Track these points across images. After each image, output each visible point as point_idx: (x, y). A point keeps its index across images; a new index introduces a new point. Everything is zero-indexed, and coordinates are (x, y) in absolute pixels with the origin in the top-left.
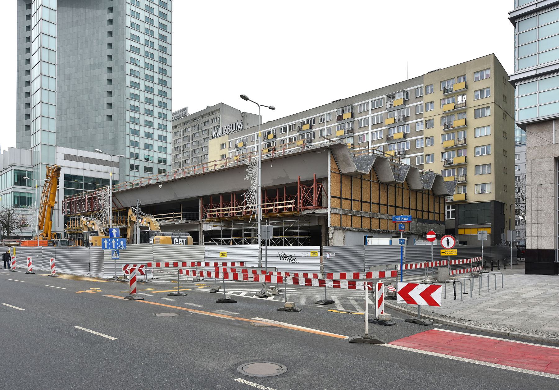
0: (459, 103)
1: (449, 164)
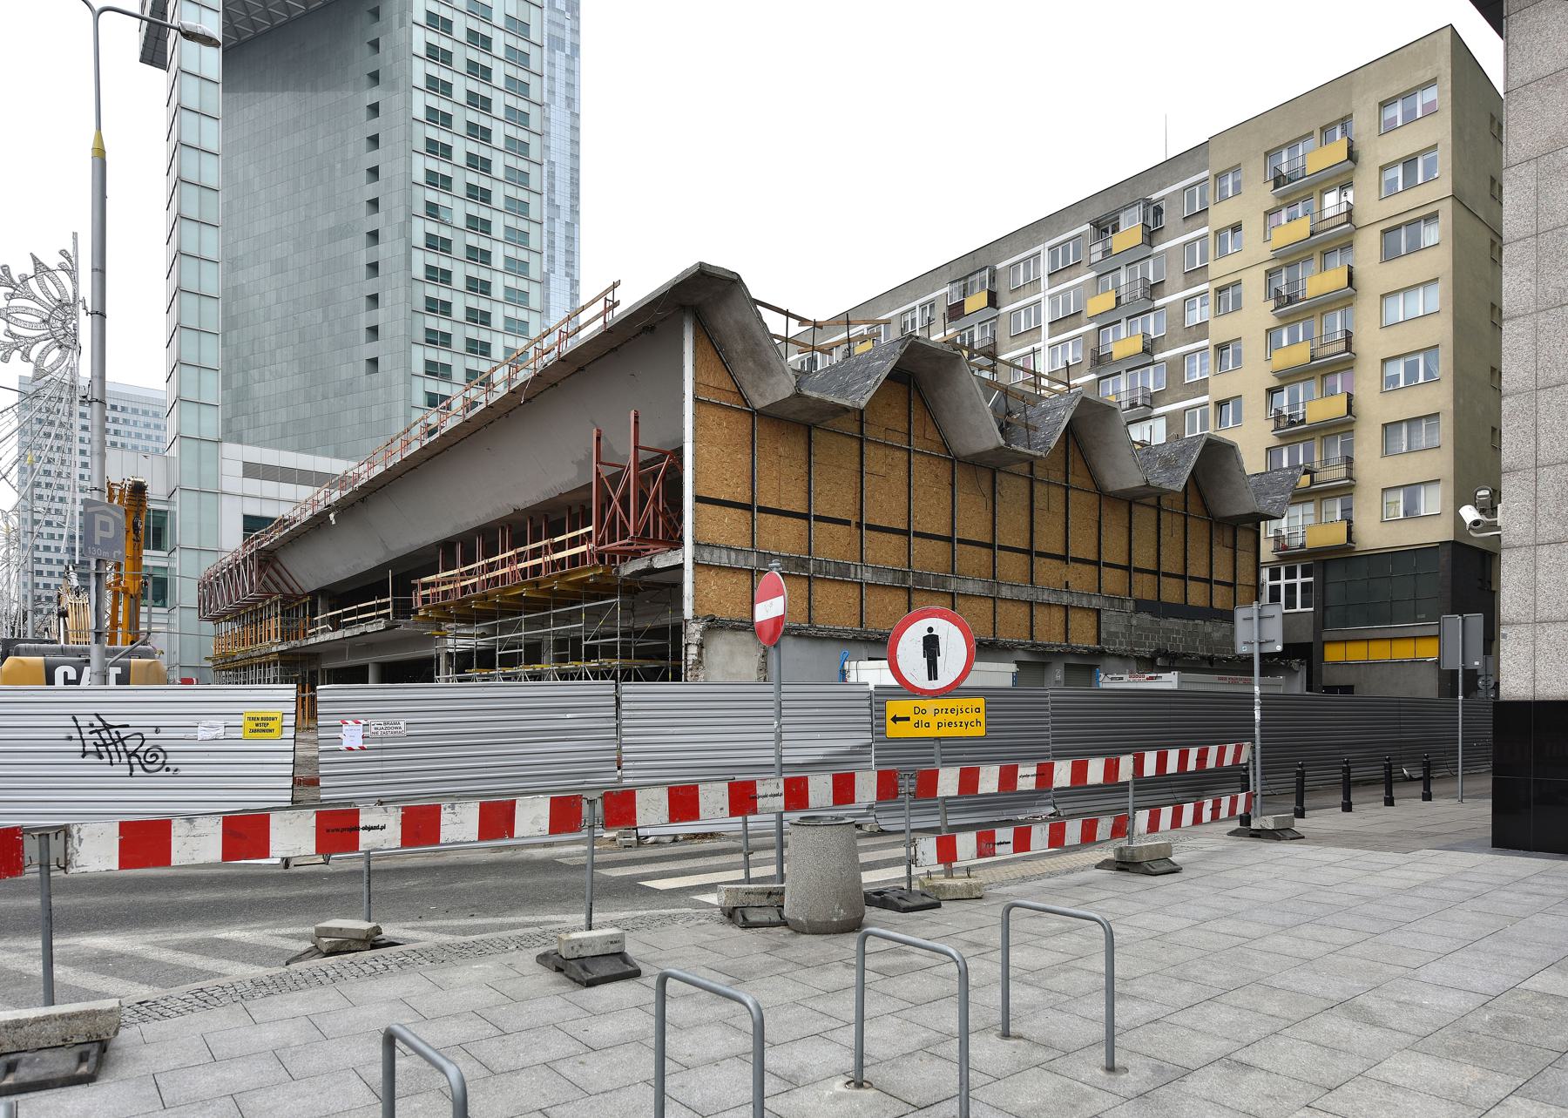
0: (1328, 214)
1: (1292, 424)
